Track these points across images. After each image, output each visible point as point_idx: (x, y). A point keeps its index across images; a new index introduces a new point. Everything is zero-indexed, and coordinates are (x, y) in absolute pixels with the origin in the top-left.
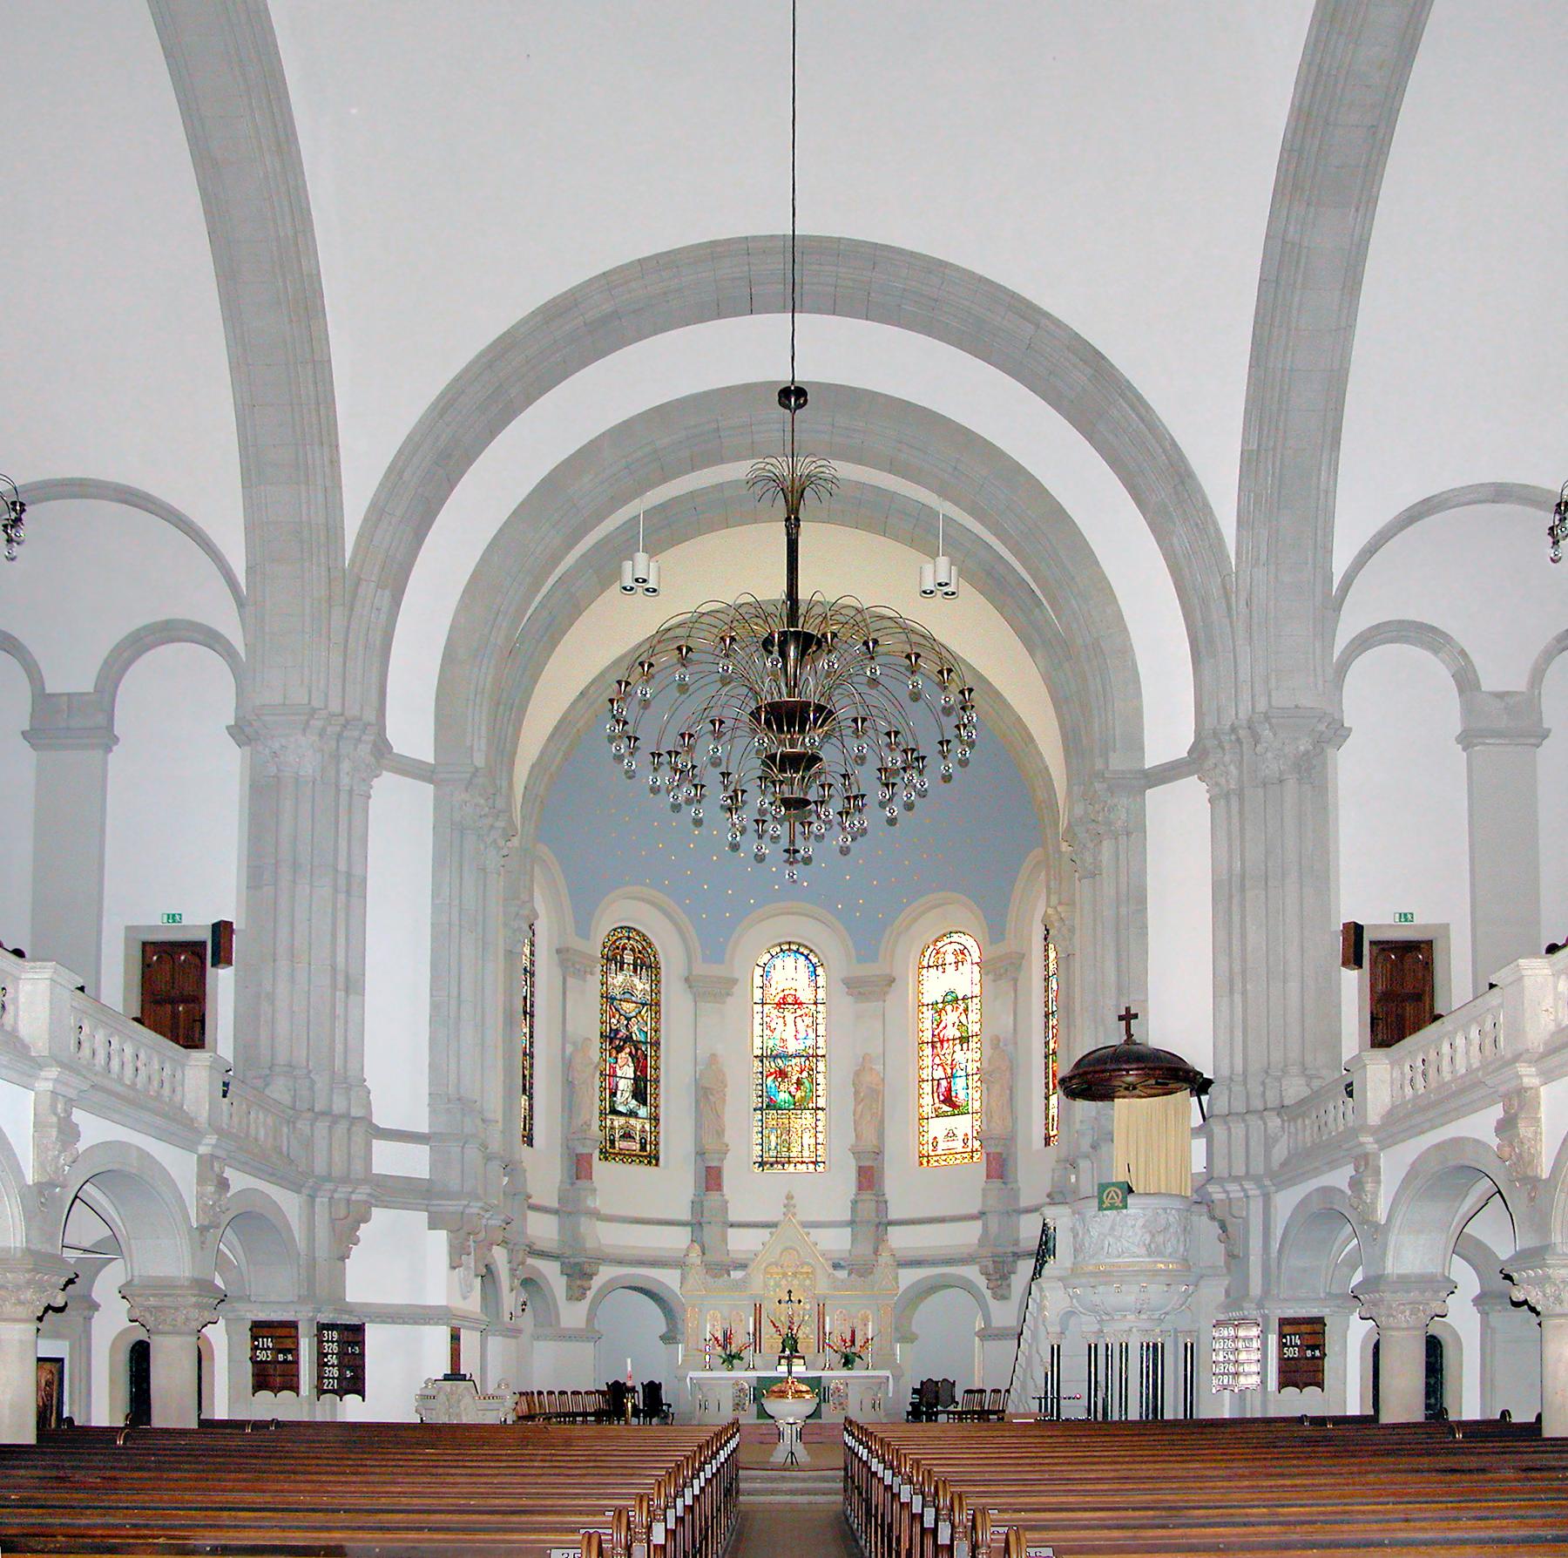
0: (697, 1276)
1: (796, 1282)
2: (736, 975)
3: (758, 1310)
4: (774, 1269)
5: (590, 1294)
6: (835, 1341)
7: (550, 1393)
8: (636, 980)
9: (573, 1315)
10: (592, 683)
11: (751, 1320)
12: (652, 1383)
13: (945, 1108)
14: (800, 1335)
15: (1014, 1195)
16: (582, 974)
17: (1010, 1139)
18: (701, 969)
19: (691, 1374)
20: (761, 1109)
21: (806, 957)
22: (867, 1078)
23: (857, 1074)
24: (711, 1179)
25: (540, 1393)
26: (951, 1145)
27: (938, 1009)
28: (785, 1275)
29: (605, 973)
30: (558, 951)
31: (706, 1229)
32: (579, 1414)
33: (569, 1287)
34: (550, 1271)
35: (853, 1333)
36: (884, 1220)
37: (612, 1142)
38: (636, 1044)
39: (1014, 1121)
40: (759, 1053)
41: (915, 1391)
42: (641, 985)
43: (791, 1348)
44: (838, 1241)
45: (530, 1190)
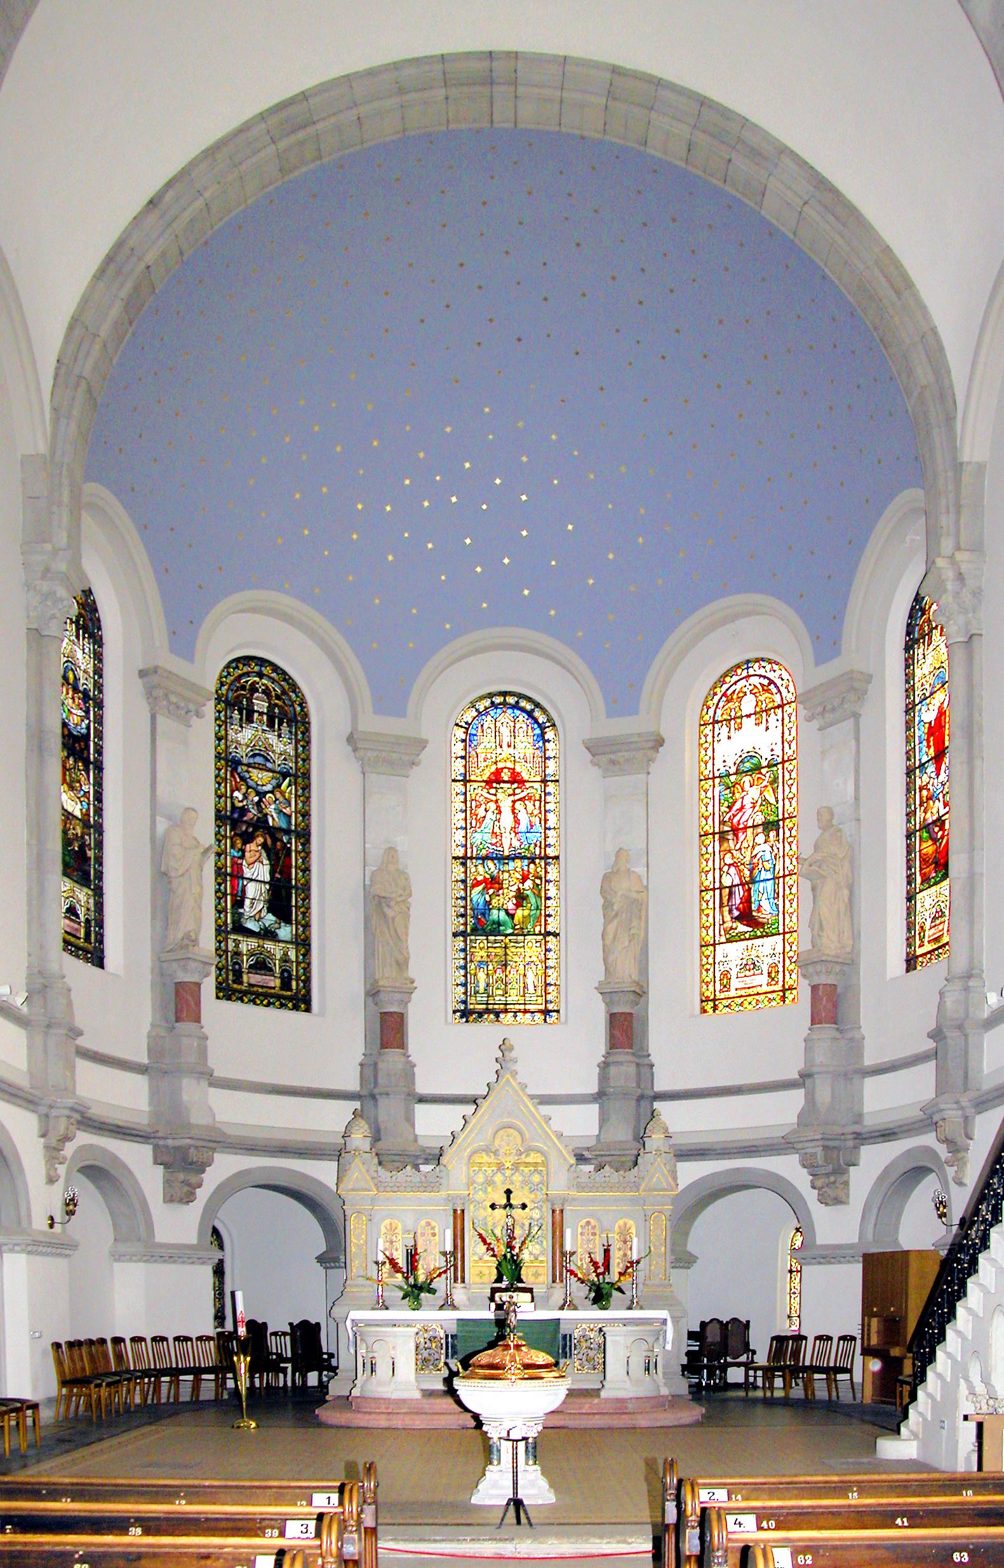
0: (361, 1171)
1: (517, 1178)
2: (424, 736)
3: (459, 1217)
4: (484, 1158)
5: (203, 1194)
6: (581, 1263)
7: (136, 1340)
8: (272, 738)
9: (179, 1225)
10: (170, 185)
11: (449, 1234)
12: (304, 1323)
13: (742, 928)
14: (525, 1256)
15: (856, 1047)
16: (185, 713)
17: (849, 964)
18: (370, 723)
19: (355, 1315)
20: (464, 934)
21: (530, 714)
22: (622, 886)
23: (606, 878)
24: (390, 1030)
25: (118, 1341)
26: (750, 981)
27: (730, 781)
28: (500, 1167)
29: (223, 723)
30: (142, 674)
31: (383, 1102)
32: (186, 1371)
33: (167, 1182)
34: (137, 1159)
35: (607, 1252)
36: (650, 1093)
37: (238, 974)
38: (273, 832)
39: (856, 936)
40: (460, 852)
41: (692, 1335)
42: (280, 745)
43: (510, 1271)
44: (583, 1122)
45: (80, 1022)
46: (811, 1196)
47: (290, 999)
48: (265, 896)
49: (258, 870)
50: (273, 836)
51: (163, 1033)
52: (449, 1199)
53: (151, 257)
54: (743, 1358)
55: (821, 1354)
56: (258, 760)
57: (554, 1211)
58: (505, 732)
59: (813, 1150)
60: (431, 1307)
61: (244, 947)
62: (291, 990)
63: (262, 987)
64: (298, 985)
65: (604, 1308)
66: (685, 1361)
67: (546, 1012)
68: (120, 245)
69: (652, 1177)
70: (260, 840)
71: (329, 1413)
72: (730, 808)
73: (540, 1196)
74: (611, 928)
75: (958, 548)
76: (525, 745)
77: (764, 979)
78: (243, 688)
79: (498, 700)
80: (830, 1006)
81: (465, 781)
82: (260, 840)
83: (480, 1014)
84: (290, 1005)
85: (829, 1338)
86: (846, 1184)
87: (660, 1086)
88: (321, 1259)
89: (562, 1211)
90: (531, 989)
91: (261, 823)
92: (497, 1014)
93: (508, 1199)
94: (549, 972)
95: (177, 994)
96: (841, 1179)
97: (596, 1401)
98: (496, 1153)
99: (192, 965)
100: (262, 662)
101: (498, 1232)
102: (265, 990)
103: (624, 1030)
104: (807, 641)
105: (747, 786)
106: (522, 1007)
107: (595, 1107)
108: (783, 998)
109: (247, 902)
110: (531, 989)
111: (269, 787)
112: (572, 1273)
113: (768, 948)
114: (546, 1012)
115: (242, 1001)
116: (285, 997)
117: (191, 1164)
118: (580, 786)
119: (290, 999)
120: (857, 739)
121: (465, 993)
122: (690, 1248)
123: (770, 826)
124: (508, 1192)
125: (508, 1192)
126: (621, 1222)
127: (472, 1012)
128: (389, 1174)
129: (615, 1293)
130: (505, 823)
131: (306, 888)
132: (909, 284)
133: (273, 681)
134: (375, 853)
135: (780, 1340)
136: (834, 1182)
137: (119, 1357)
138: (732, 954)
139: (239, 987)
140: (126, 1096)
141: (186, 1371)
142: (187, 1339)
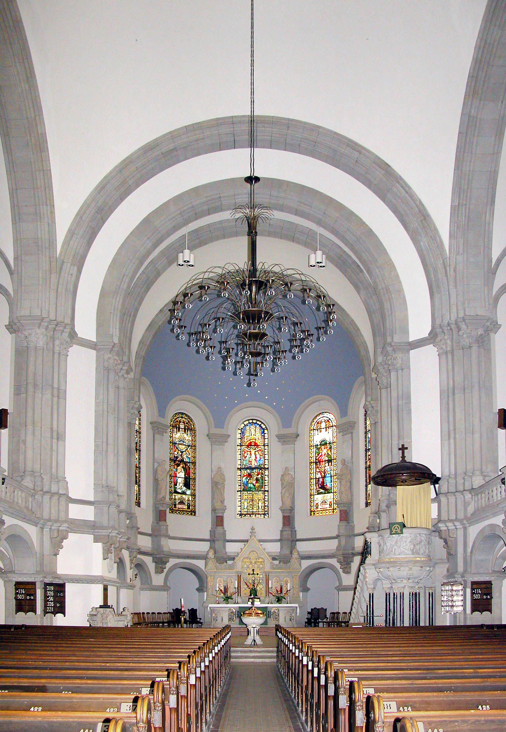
0: (212, 564)
1: (256, 566)
3: (239, 577)
5: (165, 571)
6: (274, 591)
7: (148, 613)
8: (185, 435)
9: (158, 580)
13: (322, 491)
14: (258, 588)
15: (352, 528)
17: (350, 504)
19: (210, 605)
21: (260, 425)
22: (287, 478)
23: (282, 476)
25: (143, 613)
27: (318, 448)
28: (251, 563)
30: (151, 423)
31: (217, 542)
32: (161, 623)
33: (156, 568)
37: (175, 505)
38: (186, 463)
39: (352, 496)
41: (309, 613)
42: (187, 437)
44: (275, 548)
46: (341, 571)
48: (183, 482)
49: (181, 474)
50: (185, 464)
51: (156, 524)
52: (237, 572)
53: (160, 324)
54: (325, 620)
55: (344, 618)
56: (181, 442)
58: (253, 431)
60: (232, 603)
61: (177, 497)
66: (306, 620)
67: (264, 514)
68: (153, 321)
70: (182, 466)
72: (318, 455)
73: (262, 571)
74: (283, 491)
75: (372, 400)
76: (258, 435)
77: (328, 506)
78: (177, 422)
79: (251, 421)
80: (345, 516)
81: (241, 446)
82: (182, 466)
83: (245, 515)
85: (346, 613)
86: (350, 567)
87: (299, 537)
88: (198, 590)
90: (260, 507)
91: (182, 461)
94: (266, 502)
95: (160, 513)
96: (348, 566)
98: (250, 559)
99: (165, 505)
100: (182, 414)
101: (250, 581)
103: (288, 520)
104: (338, 410)
105: (323, 449)
108: (333, 512)
109: (178, 484)
110: (260, 507)
111: (184, 450)
112: (271, 593)
113: (329, 497)
114: (264, 514)
118: (276, 446)
120: (352, 440)
122: (308, 585)
123: (329, 461)
124: (253, 570)
125: (253, 570)
127: (243, 514)
130: (253, 458)
131: (195, 479)
132: (359, 330)
133: (186, 419)
134: (214, 469)
135: (333, 613)
137: (144, 618)
138: (319, 498)
140: (145, 542)
141: (161, 623)
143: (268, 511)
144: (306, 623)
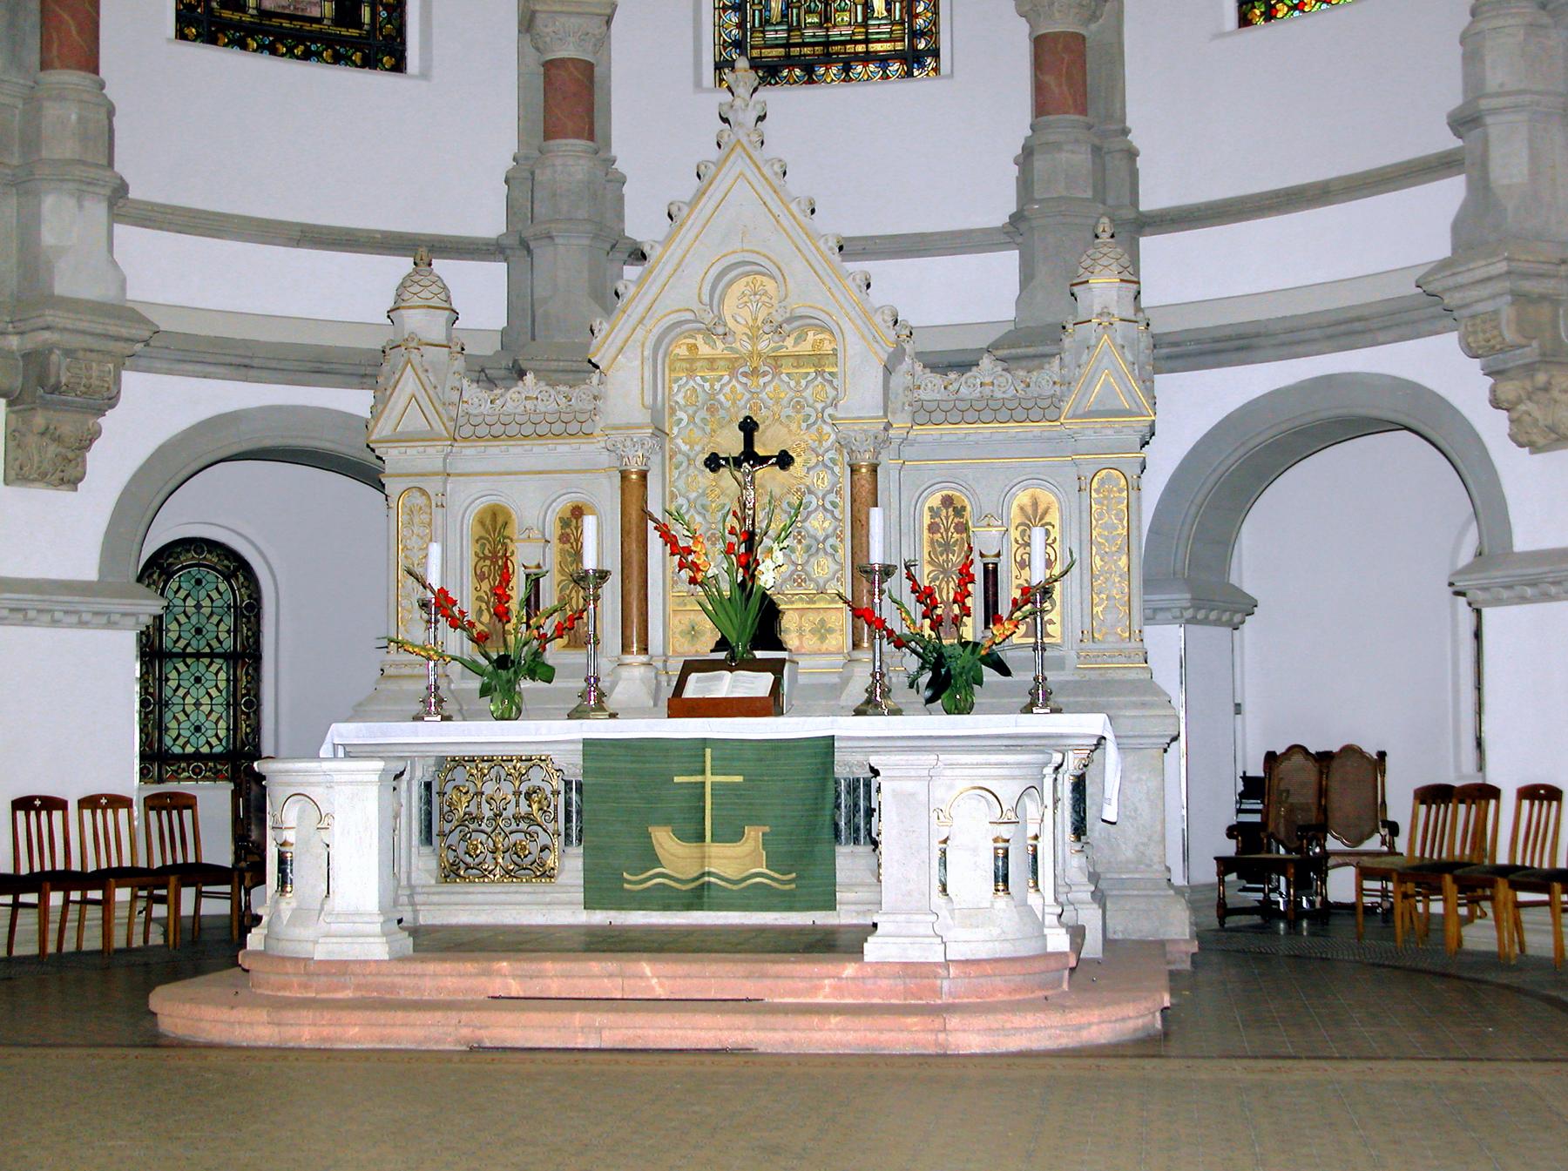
24: (568, 98)
46: (1492, 427)
47: (354, 43)
57: (854, 470)
59: (1488, 306)
62: (360, 25)
63: (291, 17)
64: (374, 14)
65: (962, 708)
66: (1229, 848)
69: (1090, 384)
71: (186, 1010)
84: (357, 57)
89: (874, 469)
92: (809, 69)
93: (749, 442)
97: (850, 969)
102: (298, 24)
106: (860, 48)
107: (1012, 257)
115: (244, 47)
116: (344, 41)
117: (56, 389)
119: (354, 43)
121: (741, 25)
126: (1023, 498)
128: (485, 395)
129: (989, 674)
136: (1546, 389)
139: (236, 16)
142: (53, 804)
143: (932, 33)
144: (1225, 865)
